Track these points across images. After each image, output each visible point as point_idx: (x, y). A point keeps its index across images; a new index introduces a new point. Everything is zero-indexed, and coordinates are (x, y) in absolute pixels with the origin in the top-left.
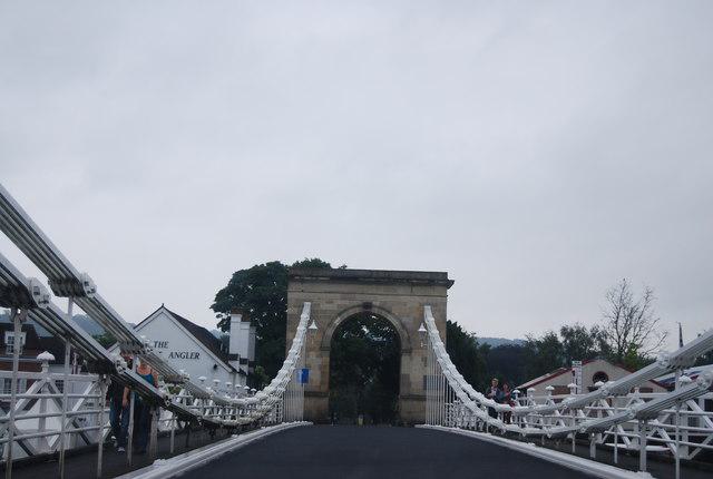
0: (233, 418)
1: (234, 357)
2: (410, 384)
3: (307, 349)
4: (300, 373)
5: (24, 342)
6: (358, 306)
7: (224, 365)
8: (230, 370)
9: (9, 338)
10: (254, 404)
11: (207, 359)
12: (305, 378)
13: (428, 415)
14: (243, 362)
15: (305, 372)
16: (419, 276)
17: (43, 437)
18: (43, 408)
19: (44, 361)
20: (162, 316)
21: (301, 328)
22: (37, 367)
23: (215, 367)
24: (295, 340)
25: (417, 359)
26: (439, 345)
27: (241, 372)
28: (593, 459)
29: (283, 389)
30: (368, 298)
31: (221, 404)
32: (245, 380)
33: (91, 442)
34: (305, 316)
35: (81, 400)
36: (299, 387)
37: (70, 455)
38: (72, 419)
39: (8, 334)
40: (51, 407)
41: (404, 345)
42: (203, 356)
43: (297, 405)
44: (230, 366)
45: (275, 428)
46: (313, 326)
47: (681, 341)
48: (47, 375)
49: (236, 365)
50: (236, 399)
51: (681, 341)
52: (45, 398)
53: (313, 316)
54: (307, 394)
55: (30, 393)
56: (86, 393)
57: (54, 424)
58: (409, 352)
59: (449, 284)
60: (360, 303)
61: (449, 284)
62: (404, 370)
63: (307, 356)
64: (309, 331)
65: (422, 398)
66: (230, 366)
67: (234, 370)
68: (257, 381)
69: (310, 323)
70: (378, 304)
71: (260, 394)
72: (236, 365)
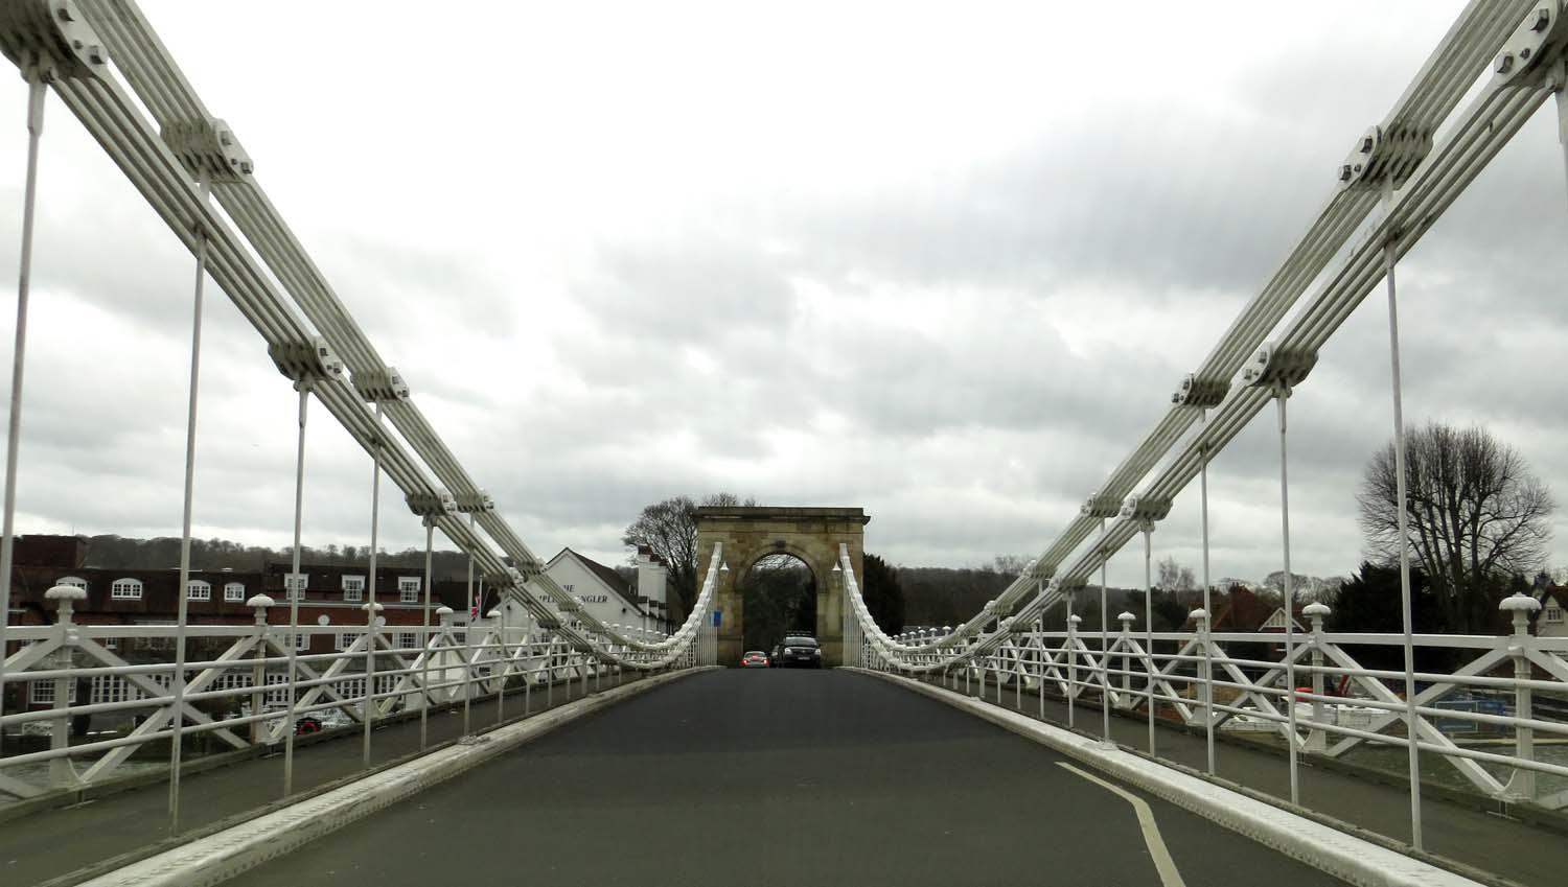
0: (646, 662)
1: (644, 600)
2: (826, 625)
3: (718, 591)
4: (712, 615)
5: (306, 585)
6: (772, 545)
7: (632, 607)
8: (640, 614)
9: (403, 583)
10: (665, 649)
11: (616, 603)
12: (717, 622)
13: (846, 657)
14: (653, 604)
15: (718, 615)
16: (833, 513)
17: (444, 688)
18: (443, 661)
19: (444, 614)
20: (566, 559)
21: (712, 570)
22: (46, 613)
23: (624, 610)
24: (706, 583)
25: (833, 600)
26: (853, 586)
27: (652, 616)
28: (955, 691)
29: (694, 634)
30: (781, 537)
31: (635, 648)
32: (664, 625)
33: (436, 702)
34: (716, 557)
35: (480, 650)
36: (711, 630)
37: (474, 703)
38: (513, 666)
39: (287, 577)
40: (453, 660)
41: (821, 586)
42: (610, 598)
43: (710, 649)
44: (640, 610)
45: (683, 672)
46: (725, 568)
47: (302, 425)
48: (446, 628)
49: (646, 608)
50: (647, 645)
51: (302, 425)
52: (445, 651)
53: (724, 558)
54: (720, 638)
55: (431, 646)
56: (484, 644)
57: (457, 675)
58: (827, 592)
59: (866, 520)
60: (773, 542)
61: (866, 520)
62: (820, 611)
63: (719, 599)
64: (720, 573)
65: (841, 639)
66: (640, 610)
67: (644, 614)
68: (672, 623)
69: (721, 564)
70: (791, 542)
71: (672, 640)
72: (646, 608)
